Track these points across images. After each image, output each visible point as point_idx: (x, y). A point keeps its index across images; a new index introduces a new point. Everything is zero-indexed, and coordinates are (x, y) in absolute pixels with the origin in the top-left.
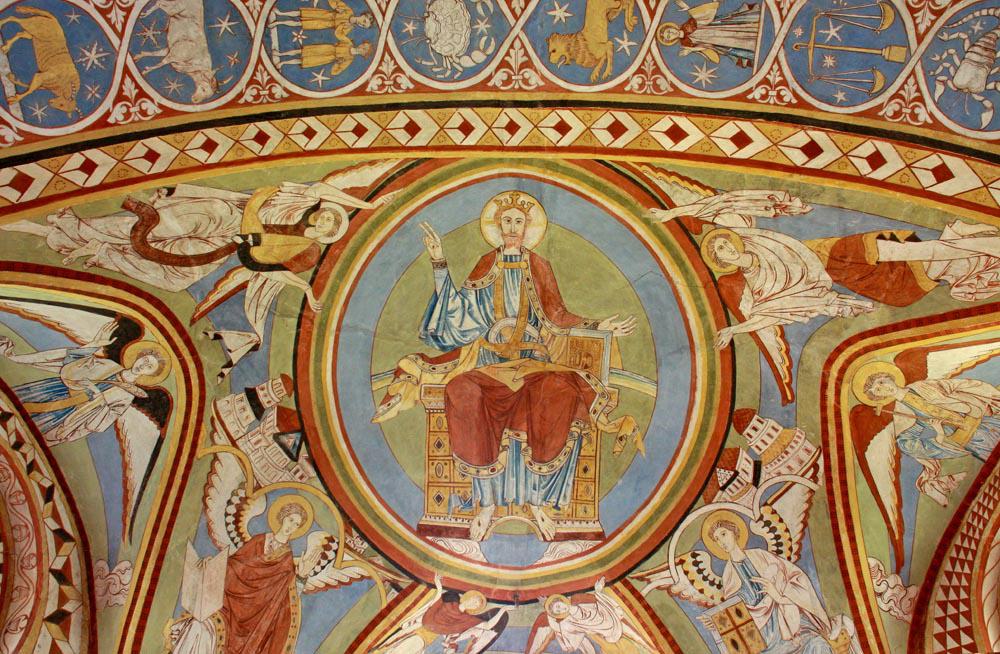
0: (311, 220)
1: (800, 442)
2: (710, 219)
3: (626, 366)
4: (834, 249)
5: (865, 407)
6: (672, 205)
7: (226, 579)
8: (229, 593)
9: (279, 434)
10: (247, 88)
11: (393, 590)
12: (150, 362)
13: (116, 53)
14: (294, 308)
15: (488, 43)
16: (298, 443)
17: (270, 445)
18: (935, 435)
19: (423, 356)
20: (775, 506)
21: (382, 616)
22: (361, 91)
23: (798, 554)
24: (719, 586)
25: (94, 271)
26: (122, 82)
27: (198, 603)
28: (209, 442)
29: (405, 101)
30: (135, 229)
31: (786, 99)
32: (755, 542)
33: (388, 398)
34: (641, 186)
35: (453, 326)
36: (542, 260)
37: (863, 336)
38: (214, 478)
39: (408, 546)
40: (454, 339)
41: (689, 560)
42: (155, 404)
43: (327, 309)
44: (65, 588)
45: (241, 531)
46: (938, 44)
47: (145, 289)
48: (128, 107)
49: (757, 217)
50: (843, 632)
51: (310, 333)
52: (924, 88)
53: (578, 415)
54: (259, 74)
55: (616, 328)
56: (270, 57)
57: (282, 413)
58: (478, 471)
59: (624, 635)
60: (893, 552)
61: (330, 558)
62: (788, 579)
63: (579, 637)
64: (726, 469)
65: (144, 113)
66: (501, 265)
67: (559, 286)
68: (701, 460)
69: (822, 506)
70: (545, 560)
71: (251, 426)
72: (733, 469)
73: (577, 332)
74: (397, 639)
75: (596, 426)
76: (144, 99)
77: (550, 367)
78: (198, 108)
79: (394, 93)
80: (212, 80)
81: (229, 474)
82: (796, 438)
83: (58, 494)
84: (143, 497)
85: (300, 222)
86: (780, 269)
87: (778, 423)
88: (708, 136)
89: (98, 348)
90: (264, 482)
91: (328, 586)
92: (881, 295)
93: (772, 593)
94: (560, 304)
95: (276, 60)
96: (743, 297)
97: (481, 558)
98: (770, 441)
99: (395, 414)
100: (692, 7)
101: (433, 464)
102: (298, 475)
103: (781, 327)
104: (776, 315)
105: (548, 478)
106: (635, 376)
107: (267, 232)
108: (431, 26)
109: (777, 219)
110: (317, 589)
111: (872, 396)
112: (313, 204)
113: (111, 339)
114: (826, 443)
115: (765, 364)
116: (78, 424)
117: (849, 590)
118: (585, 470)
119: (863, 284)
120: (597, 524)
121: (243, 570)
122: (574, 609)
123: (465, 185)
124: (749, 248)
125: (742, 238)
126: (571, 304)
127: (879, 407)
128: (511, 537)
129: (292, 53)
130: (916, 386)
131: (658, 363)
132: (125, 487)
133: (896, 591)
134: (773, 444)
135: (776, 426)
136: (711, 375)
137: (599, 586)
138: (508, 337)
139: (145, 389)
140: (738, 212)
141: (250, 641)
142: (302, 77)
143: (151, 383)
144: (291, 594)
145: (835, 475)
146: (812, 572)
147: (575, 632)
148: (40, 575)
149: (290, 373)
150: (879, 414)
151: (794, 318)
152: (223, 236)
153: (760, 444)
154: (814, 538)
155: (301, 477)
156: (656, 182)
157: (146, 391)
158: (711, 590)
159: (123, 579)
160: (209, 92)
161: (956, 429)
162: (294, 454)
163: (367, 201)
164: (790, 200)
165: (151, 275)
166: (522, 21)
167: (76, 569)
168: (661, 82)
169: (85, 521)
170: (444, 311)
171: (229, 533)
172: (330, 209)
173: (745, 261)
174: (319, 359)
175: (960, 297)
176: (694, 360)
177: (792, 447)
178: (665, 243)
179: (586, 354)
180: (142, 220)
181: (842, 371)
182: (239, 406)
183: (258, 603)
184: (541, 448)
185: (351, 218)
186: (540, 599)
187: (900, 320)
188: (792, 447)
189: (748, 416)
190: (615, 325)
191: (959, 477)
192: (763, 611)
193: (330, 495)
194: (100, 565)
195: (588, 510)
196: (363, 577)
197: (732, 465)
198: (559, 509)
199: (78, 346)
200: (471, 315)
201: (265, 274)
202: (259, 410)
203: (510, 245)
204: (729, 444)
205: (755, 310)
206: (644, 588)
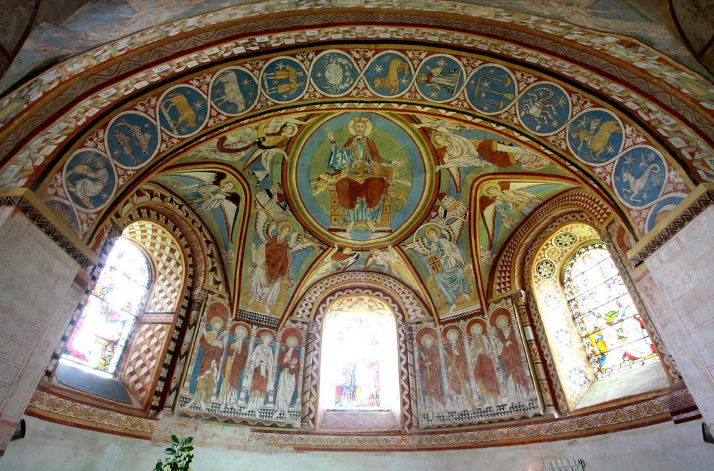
4: (480, 144)
6: (421, 123)
8: (267, 256)
12: (230, 184)
13: (206, 101)
15: (350, 80)
18: (510, 207)
19: (328, 173)
21: (318, 258)
22: (301, 99)
24: (430, 249)
25: (205, 160)
30: (218, 143)
32: (443, 236)
33: (316, 187)
37: (488, 174)
41: (420, 240)
42: (234, 198)
43: (292, 160)
44: (213, 259)
46: (526, 96)
47: (225, 162)
51: (286, 168)
52: (518, 111)
56: (265, 91)
57: (279, 195)
65: (221, 120)
71: (269, 201)
73: (384, 164)
77: (374, 176)
78: (241, 114)
81: (262, 218)
83: (204, 229)
86: (460, 148)
91: (299, 250)
93: (447, 253)
94: (378, 155)
95: (267, 92)
97: (350, 238)
100: (431, 68)
108: (327, 74)
111: (488, 193)
114: (470, 207)
115: (451, 180)
117: (472, 256)
119: (490, 158)
126: (382, 155)
127: (491, 197)
129: (273, 89)
130: (505, 191)
131: (412, 175)
136: (432, 181)
137: (390, 247)
138: (358, 166)
139: (230, 193)
142: (278, 96)
145: (472, 218)
148: (204, 257)
149: (280, 182)
158: (427, 250)
159: (232, 255)
160: (243, 107)
161: (517, 206)
165: (226, 157)
166: (363, 72)
167: (215, 251)
168: (417, 95)
169: (214, 235)
173: (447, 144)
174: (291, 176)
175: (524, 168)
178: (418, 136)
179: (387, 172)
181: (478, 185)
184: (370, 203)
191: (516, 221)
193: (298, 220)
194: (223, 250)
196: (311, 246)
197: (437, 210)
200: (345, 159)
202: (271, 196)
204: (436, 204)
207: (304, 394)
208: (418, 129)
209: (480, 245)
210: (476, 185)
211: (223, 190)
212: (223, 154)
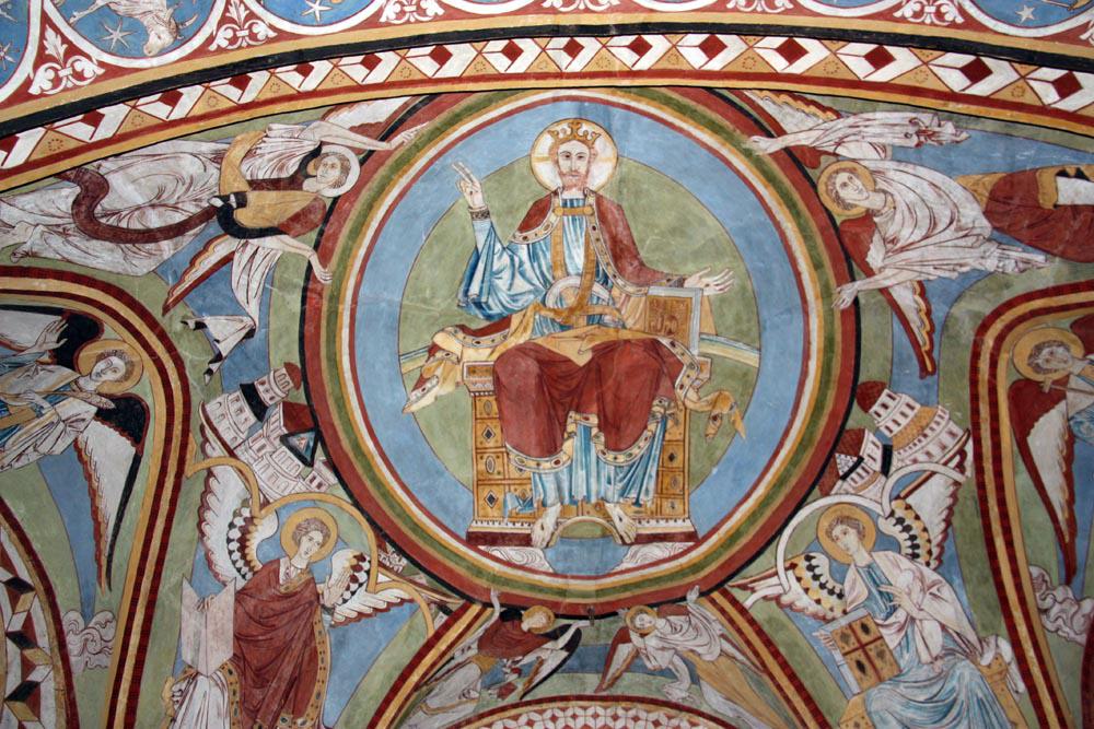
0: (310, 169)
1: (943, 423)
2: (831, 149)
3: (721, 329)
5: (1028, 381)
6: (781, 132)
7: (235, 619)
8: (239, 637)
9: (286, 436)
10: (218, 30)
11: (441, 614)
14: (295, 280)
16: (312, 444)
17: (277, 450)
20: (910, 500)
23: (939, 558)
24: (840, 596)
25: (26, 263)
26: (42, 37)
27: (202, 655)
28: (201, 456)
29: (434, 32)
30: (77, 203)
31: (948, 18)
32: (885, 543)
33: (421, 382)
34: (741, 110)
35: (500, 290)
36: (613, 203)
38: (211, 499)
39: (457, 559)
40: (502, 304)
41: (803, 564)
42: (126, 415)
43: (339, 279)
45: (248, 558)
47: (100, 277)
48: (56, 70)
49: (893, 146)
50: (998, 656)
53: (662, 391)
54: (232, 9)
55: (707, 285)
57: (290, 410)
58: (538, 465)
59: (723, 653)
60: (1061, 556)
61: (361, 581)
62: (926, 588)
63: (668, 654)
64: (847, 454)
65: (79, 76)
66: (560, 211)
67: (635, 235)
68: (816, 444)
69: (969, 503)
70: (624, 566)
71: (252, 430)
72: (857, 454)
74: (449, 671)
75: (684, 404)
76: (77, 57)
77: (625, 335)
78: (155, 62)
79: (417, 21)
80: (170, 22)
81: (228, 491)
82: (937, 419)
84: (122, 531)
85: (296, 172)
86: (922, 213)
87: (914, 399)
88: (835, 54)
89: (43, 354)
90: (273, 495)
91: (361, 615)
92: (1056, 248)
93: (907, 606)
94: (636, 256)
96: (872, 246)
98: (904, 422)
99: (433, 400)
101: (482, 458)
102: (316, 483)
103: (920, 283)
104: (915, 268)
105: (626, 469)
106: (731, 342)
107: (255, 189)
109: (920, 150)
110: (348, 620)
111: (1037, 369)
112: (312, 148)
113: (58, 342)
114: (976, 425)
115: (897, 326)
116: (26, 446)
118: (671, 458)
120: (688, 521)
121: (256, 607)
122: (661, 623)
123: (510, 114)
124: (882, 185)
125: (873, 172)
127: (1047, 381)
128: (581, 540)
132: (96, 519)
133: (1066, 606)
134: (908, 425)
135: (912, 403)
139: (111, 397)
140: (869, 140)
141: (271, 691)
143: (118, 390)
144: (317, 629)
145: (988, 466)
146: (957, 581)
147: (663, 649)
149: (296, 360)
150: (1047, 390)
151: (939, 273)
152: (195, 200)
153: (891, 425)
154: (959, 539)
155: (320, 486)
156: (761, 103)
157: (112, 400)
160: (167, 39)
162: (309, 459)
163: (382, 140)
164: (939, 126)
165: (103, 257)
170: (487, 274)
171: (234, 563)
172: (335, 154)
173: (876, 201)
176: (807, 323)
177: (932, 429)
178: (770, 179)
179: (669, 314)
180: (86, 189)
182: (237, 405)
183: (277, 644)
184: (616, 431)
185: (362, 163)
186: (621, 612)
187: (1083, 280)
188: (932, 429)
189: (875, 390)
190: (706, 280)
192: (896, 626)
193: (356, 504)
195: (676, 506)
196: (403, 601)
198: (640, 506)
199: (14, 353)
200: (523, 274)
201: (255, 242)
202: (260, 410)
203: (570, 187)
204: (851, 424)
205: (887, 262)
206: (747, 599)
208: (774, 155)
209: (1029, 564)
210: (989, 341)
211: (89, 385)
212: (96, 245)
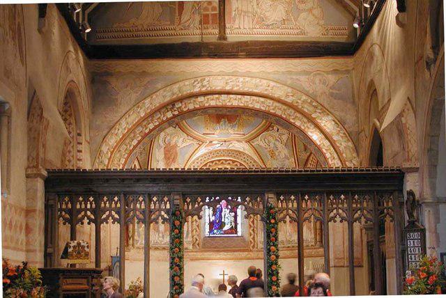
93: (280, 150)
207: (192, 231)
